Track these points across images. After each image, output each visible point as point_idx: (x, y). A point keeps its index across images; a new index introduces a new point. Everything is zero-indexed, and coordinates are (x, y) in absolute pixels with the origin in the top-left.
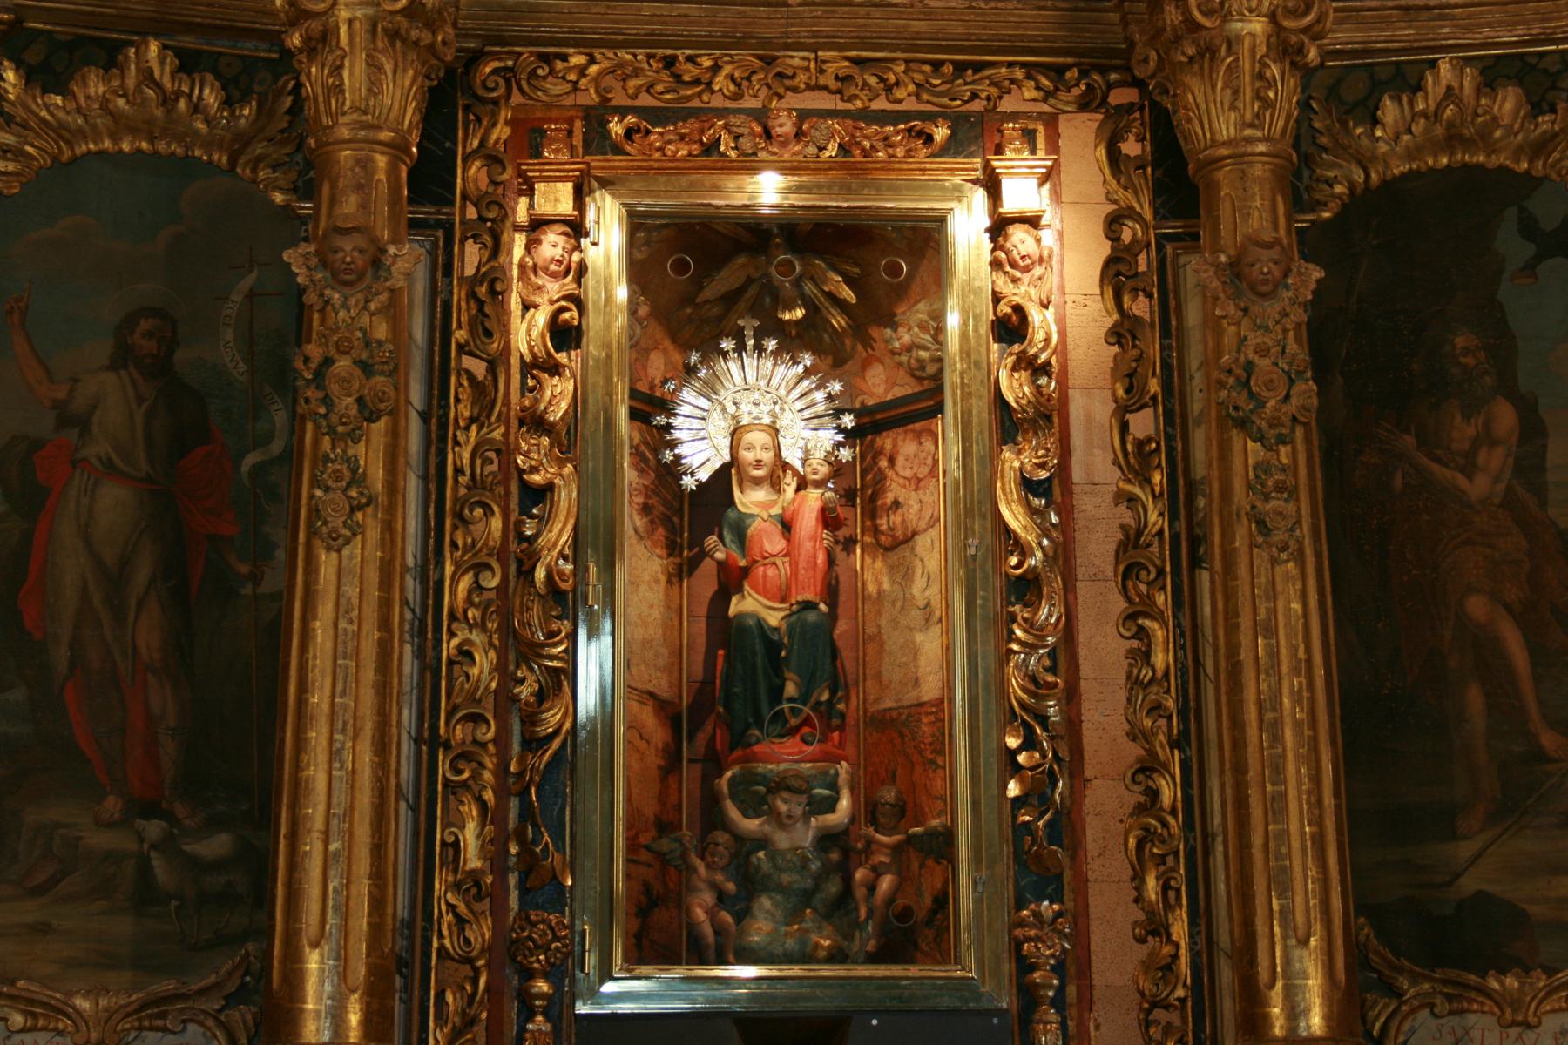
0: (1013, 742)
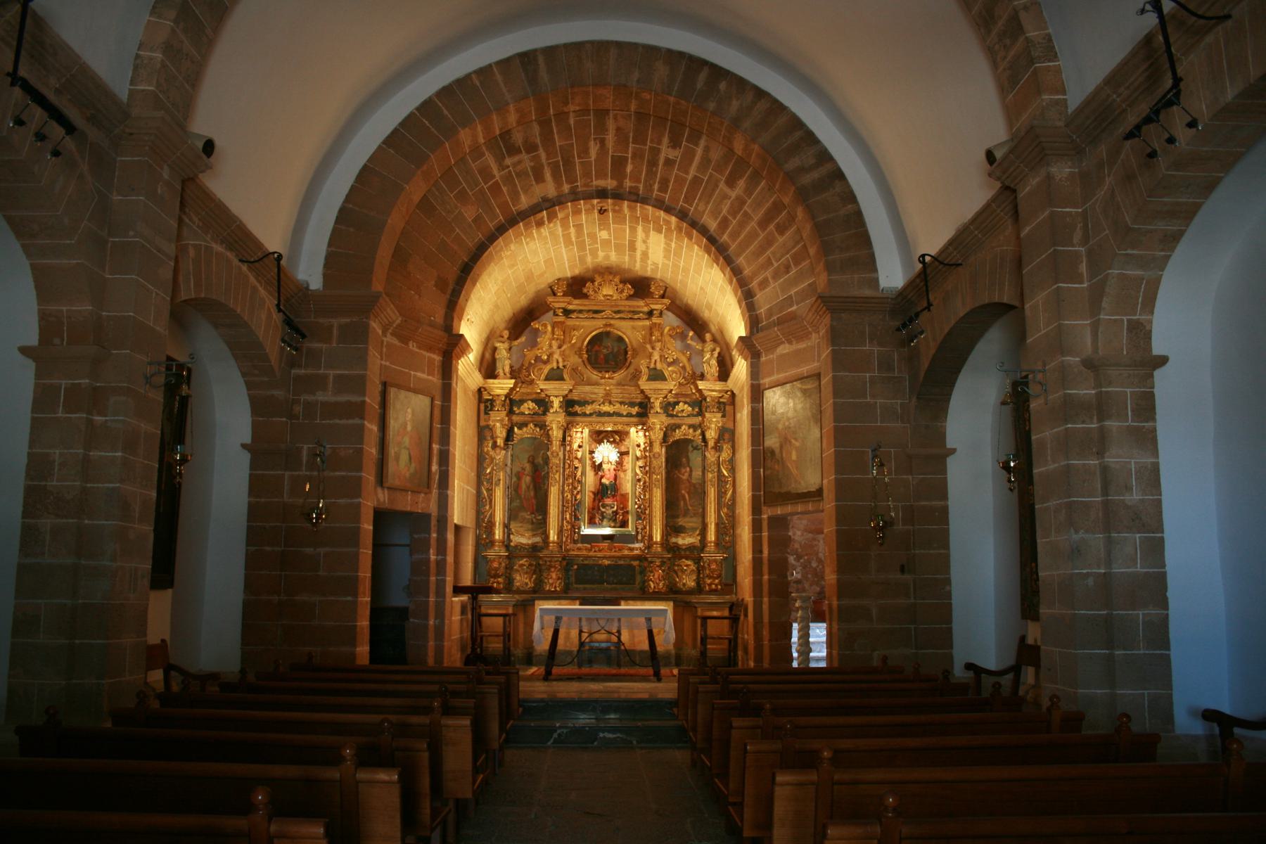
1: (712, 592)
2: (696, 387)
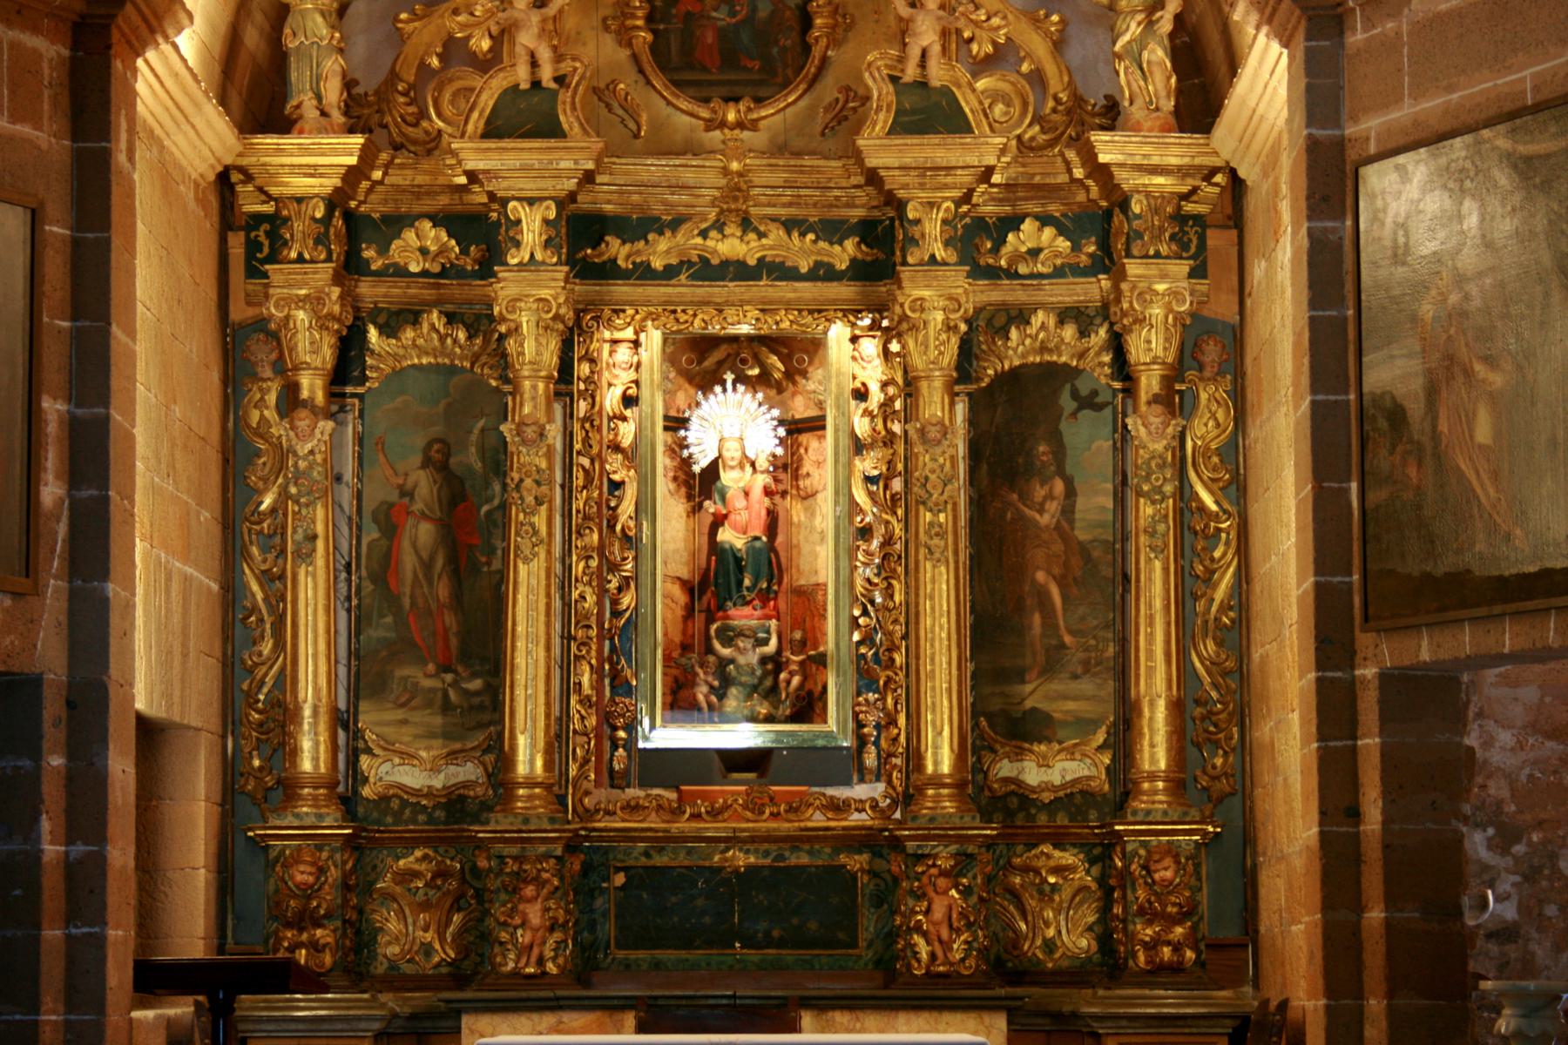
0: (857, 613)
1: (1163, 974)
2: (1089, 155)
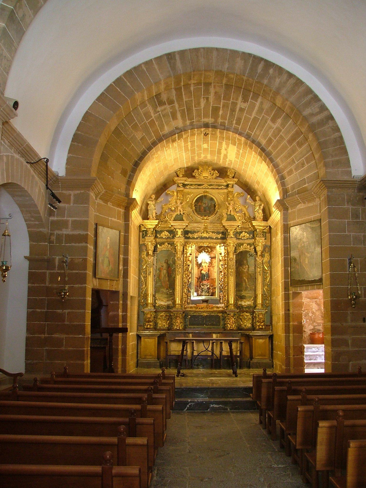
1: (260, 329)
2: (252, 224)
